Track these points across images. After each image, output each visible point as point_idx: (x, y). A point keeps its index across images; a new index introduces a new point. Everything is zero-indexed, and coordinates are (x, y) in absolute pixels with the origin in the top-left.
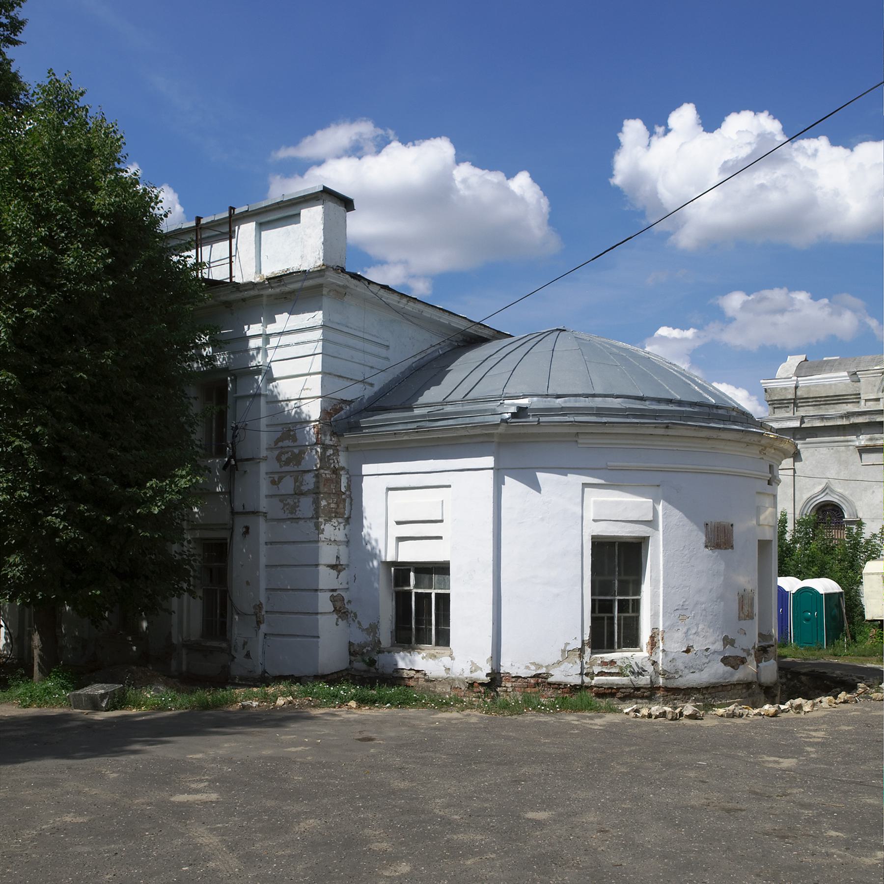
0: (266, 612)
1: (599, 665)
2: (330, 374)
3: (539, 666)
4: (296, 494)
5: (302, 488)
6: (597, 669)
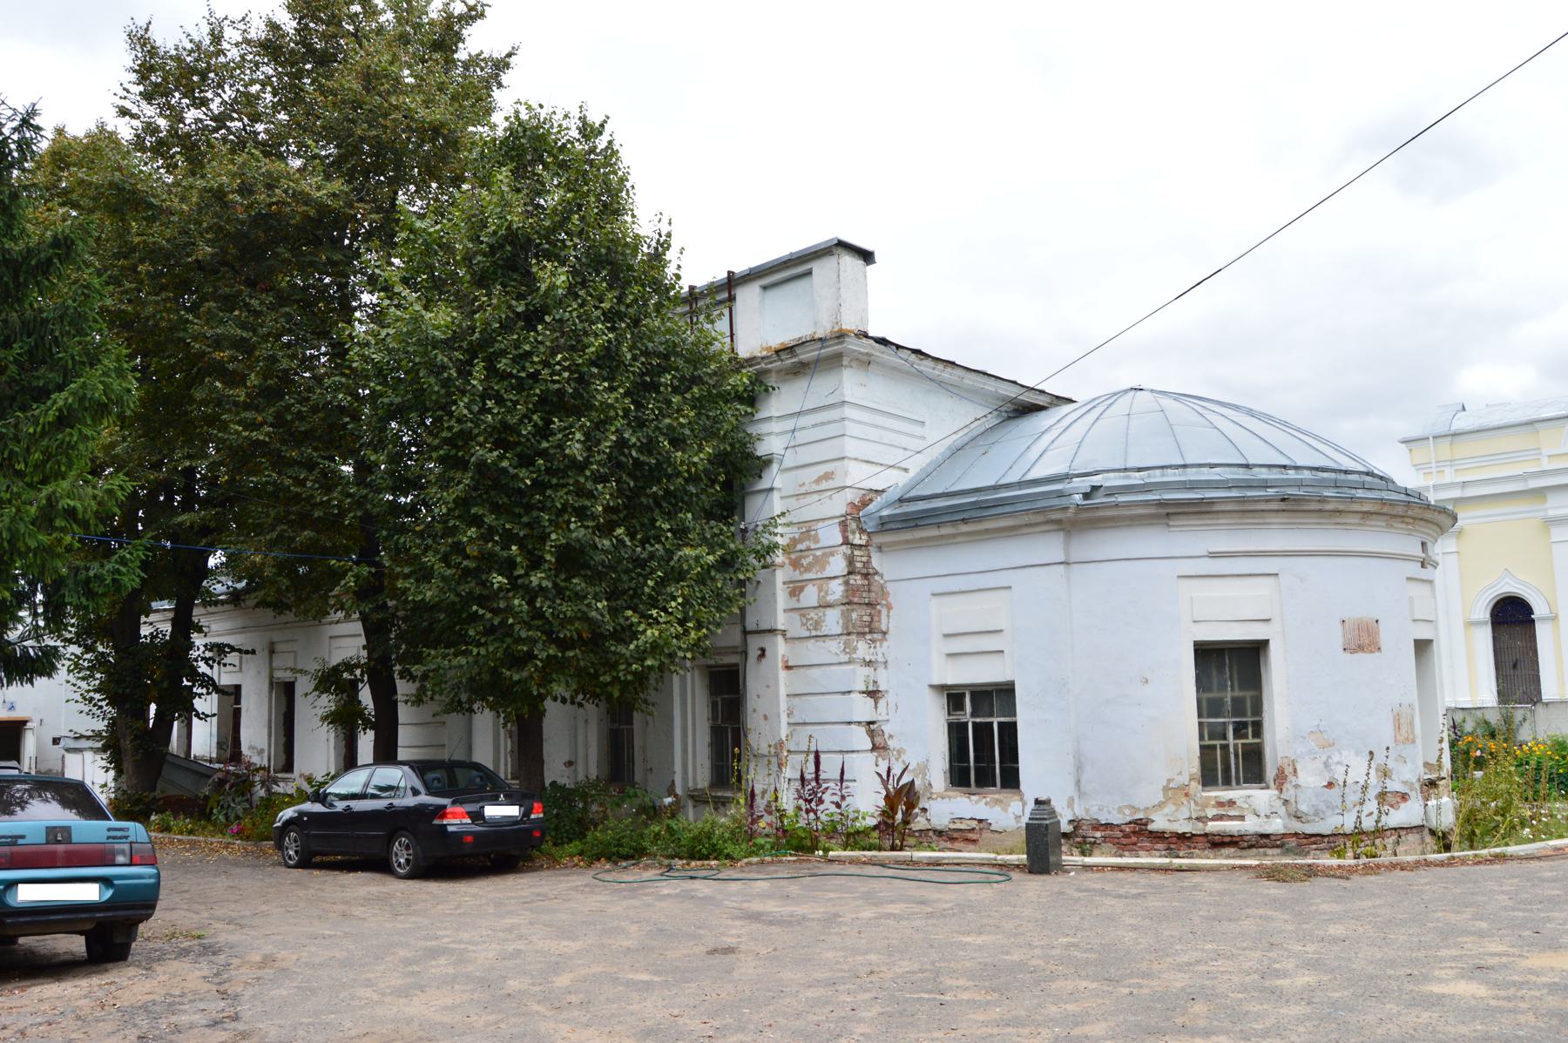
0: (789, 751)
1: (1214, 806)
2: (868, 462)
3: (1135, 809)
4: (820, 606)
5: (829, 598)
6: (1211, 812)
